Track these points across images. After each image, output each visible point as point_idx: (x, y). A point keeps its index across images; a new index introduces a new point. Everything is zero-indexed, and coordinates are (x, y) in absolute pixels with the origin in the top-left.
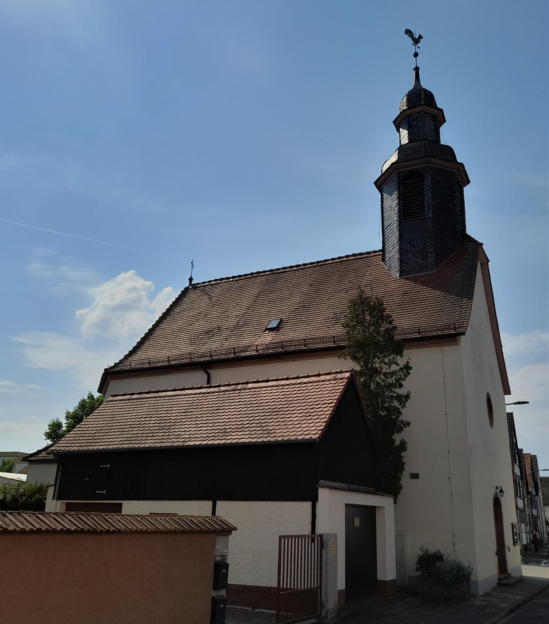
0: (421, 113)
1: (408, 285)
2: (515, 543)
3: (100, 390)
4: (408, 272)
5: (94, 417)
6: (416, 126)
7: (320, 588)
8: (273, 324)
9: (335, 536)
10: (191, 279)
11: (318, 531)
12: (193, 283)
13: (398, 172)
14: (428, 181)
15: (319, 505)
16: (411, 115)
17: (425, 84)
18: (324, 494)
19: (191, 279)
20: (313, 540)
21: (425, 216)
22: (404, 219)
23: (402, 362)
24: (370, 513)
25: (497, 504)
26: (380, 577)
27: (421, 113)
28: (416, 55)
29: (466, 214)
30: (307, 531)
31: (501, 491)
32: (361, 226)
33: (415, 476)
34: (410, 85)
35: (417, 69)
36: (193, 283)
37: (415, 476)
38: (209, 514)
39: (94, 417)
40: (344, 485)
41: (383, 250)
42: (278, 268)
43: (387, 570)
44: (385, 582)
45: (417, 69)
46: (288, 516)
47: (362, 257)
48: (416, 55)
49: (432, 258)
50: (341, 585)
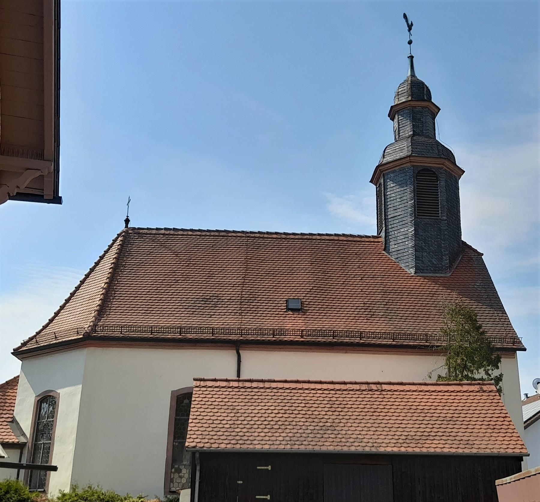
0: (417, 107)
1: (419, 281)
4: (423, 270)
5: (101, 268)
6: (420, 119)
10: (127, 221)
13: (413, 166)
16: (415, 107)
17: (420, 76)
19: (127, 221)
21: (439, 217)
22: (418, 215)
23: (495, 373)
27: (417, 107)
28: (410, 42)
29: (461, 222)
39: (101, 268)
42: (270, 231)
47: (311, 237)
48: (410, 42)
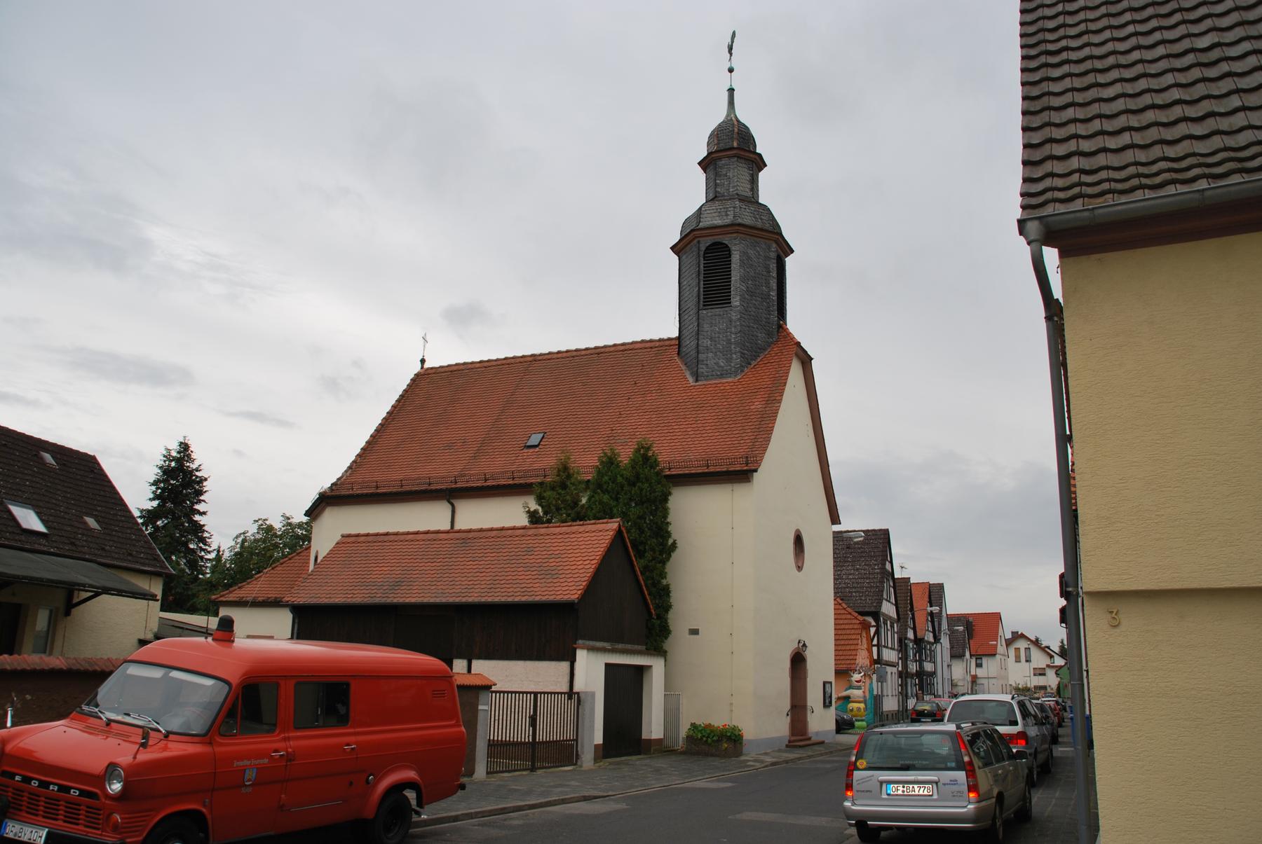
2: (827, 704)
3: (307, 514)
7: (577, 740)
8: (535, 439)
9: (593, 694)
10: (423, 361)
11: (576, 689)
12: (426, 366)
14: (736, 258)
15: (578, 665)
18: (581, 655)
19: (423, 361)
20: (570, 698)
24: (640, 671)
25: (798, 661)
26: (644, 736)
27: (732, 153)
30: (565, 688)
31: (804, 645)
32: (649, 309)
33: (694, 632)
34: (719, 116)
35: (731, 91)
36: (426, 366)
37: (694, 632)
38: (465, 671)
40: (607, 645)
41: (679, 338)
43: (654, 727)
44: (650, 741)
45: (731, 91)
46: (542, 675)
49: (736, 359)
50: (599, 738)
